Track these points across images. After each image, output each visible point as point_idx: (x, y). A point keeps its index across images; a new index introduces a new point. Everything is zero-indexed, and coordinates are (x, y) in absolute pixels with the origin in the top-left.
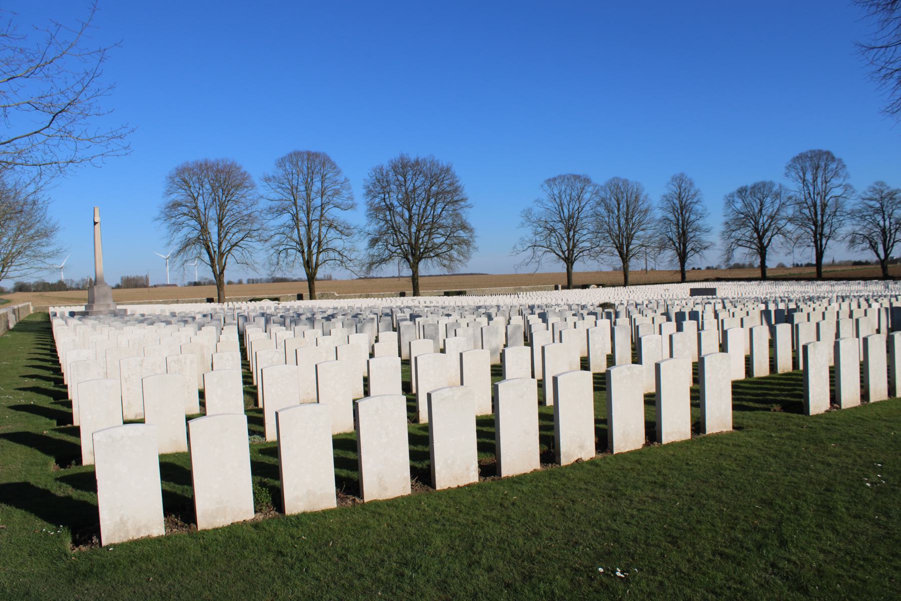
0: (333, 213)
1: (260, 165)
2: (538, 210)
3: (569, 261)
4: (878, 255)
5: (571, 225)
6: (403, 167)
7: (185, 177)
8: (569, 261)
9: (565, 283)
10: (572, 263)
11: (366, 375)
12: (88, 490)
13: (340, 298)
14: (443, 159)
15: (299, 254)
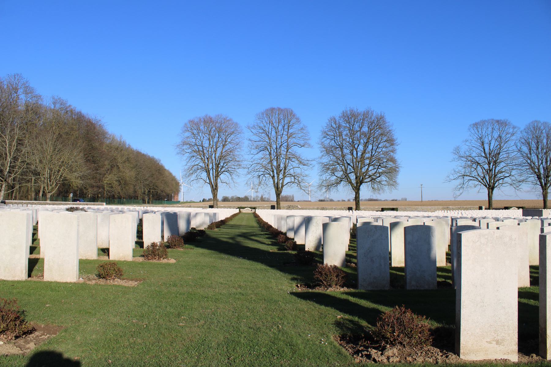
0: (295, 150)
1: (245, 117)
2: (464, 149)
3: (491, 188)
4: (489, 167)
5: (493, 159)
6: (350, 117)
7: (194, 127)
8: (491, 188)
9: (487, 207)
10: (493, 189)
11: (536, 263)
12: (524, 304)
13: (302, 209)
14: (377, 110)
15: (271, 180)
